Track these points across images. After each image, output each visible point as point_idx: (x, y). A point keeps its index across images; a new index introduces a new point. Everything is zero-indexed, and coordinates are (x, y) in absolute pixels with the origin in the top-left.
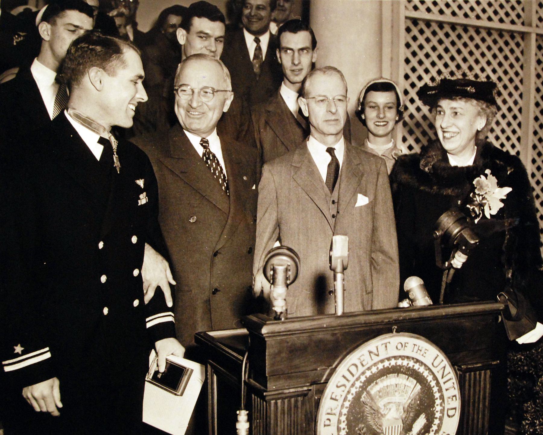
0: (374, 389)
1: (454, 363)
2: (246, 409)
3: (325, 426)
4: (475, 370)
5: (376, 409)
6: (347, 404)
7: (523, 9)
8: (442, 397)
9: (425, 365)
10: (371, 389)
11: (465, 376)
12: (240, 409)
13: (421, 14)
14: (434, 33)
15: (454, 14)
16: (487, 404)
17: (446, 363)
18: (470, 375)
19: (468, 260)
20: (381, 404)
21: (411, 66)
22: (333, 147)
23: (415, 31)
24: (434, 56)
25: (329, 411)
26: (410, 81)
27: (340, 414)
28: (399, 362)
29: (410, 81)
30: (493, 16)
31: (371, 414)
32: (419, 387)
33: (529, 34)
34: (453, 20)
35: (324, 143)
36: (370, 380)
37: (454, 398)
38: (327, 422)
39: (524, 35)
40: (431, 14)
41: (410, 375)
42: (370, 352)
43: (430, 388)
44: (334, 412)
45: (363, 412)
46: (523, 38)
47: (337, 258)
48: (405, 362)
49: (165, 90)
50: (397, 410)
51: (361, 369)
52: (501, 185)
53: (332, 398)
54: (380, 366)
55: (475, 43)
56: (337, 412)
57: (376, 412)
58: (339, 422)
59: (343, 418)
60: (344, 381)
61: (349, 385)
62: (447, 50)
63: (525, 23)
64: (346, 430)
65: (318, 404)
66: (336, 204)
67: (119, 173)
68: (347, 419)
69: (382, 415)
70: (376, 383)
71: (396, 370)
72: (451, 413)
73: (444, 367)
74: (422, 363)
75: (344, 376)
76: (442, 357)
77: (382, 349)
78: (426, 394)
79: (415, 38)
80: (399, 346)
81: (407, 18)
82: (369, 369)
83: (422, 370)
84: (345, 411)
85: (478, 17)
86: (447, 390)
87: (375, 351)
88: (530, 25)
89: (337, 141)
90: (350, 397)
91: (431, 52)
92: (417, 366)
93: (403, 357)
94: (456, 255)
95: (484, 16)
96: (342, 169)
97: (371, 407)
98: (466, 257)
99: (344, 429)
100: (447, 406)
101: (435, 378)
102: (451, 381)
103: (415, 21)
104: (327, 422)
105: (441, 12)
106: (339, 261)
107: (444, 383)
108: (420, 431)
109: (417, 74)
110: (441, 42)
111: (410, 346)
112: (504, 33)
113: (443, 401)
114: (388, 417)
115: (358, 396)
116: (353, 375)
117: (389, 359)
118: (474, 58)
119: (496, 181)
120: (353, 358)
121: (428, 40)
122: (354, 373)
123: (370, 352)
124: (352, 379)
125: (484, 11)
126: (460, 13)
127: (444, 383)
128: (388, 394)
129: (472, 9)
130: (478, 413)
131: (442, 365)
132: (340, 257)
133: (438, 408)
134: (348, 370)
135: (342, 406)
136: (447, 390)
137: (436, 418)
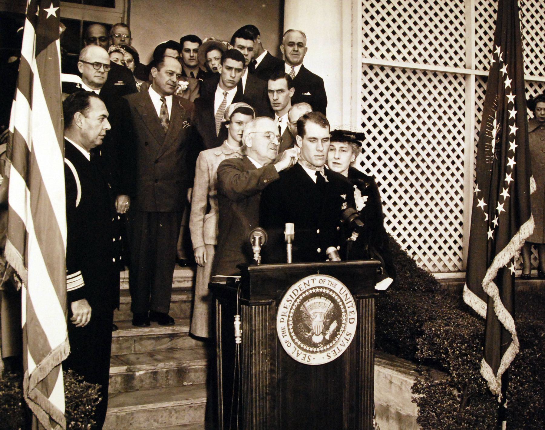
0: (307, 304)
1: (353, 293)
2: (239, 314)
3: (283, 336)
4: (366, 298)
5: (308, 315)
6: (293, 311)
8: (346, 312)
9: (336, 293)
10: (306, 304)
11: (360, 302)
12: (236, 314)
13: (377, 60)
14: (388, 76)
16: (373, 318)
17: (348, 292)
18: (363, 301)
19: (359, 236)
20: (311, 312)
23: (371, 74)
25: (283, 314)
26: (367, 116)
27: (289, 316)
28: (321, 290)
29: (367, 116)
31: (306, 318)
32: (332, 305)
36: (305, 299)
37: (353, 313)
38: (282, 320)
39: (465, 77)
41: (327, 298)
42: (305, 284)
43: (339, 306)
44: (285, 314)
45: (301, 316)
46: (464, 78)
47: (288, 235)
48: (324, 291)
50: (321, 317)
51: (300, 293)
52: (363, 195)
53: (284, 307)
54: (311, 292)
56: (287, 314)
57: (308, 317)
58: (288, 321)
59: (291, 319)
60: (290, 298)
61: (293, 300)
63: (466, 66)
64: (292, 325)
65: (277, 310)
67: (327, 181)
68: (293, 319)
69: (312, 319)
70: (309, 301)
71: (319, 294)
72: (352, 321)
73: (347, 295)
74: (334, 292)
75: (290, 296)
76: (345, 288)
77: (311, 282)
78: (337, 309)
79: (371, 80)
80: (321, 281)
82: (304, 292)
83: (334, 295)
84: (291, 315)
86: (348, 307)
87: (307, 283)
88: (470, 68)
90: (294, 307)
92: (331, 293)
93: (323, 288)
94: (353, 234)
97: (306, 314)
98: (358, 234)
99: (291, 325)
100: (349, 317)
101: (342, 300)
102: (351, 303)
103: (371, 67)
104: (282, 320)
106: (289, 237)
107: (347, 303)
108: (334, 330)
111: (327, 282)
113: (347, 314)
114: (315, 320)
115: (298, 307)
116: (296, 296)
117: (315, 288)
119: (360, 192)
120: (295, 286)
122: (296, 294)
123: (305, 284)
124: (295, 298)
127: (347, 303)
128: (315, 308)
130: (368, 324)
131: (345, 293)
132: (289, 235)
133: (344, 318)
134: (293, 292)
135: (290, 312)
136: (348, 307)
137: (343, 323)
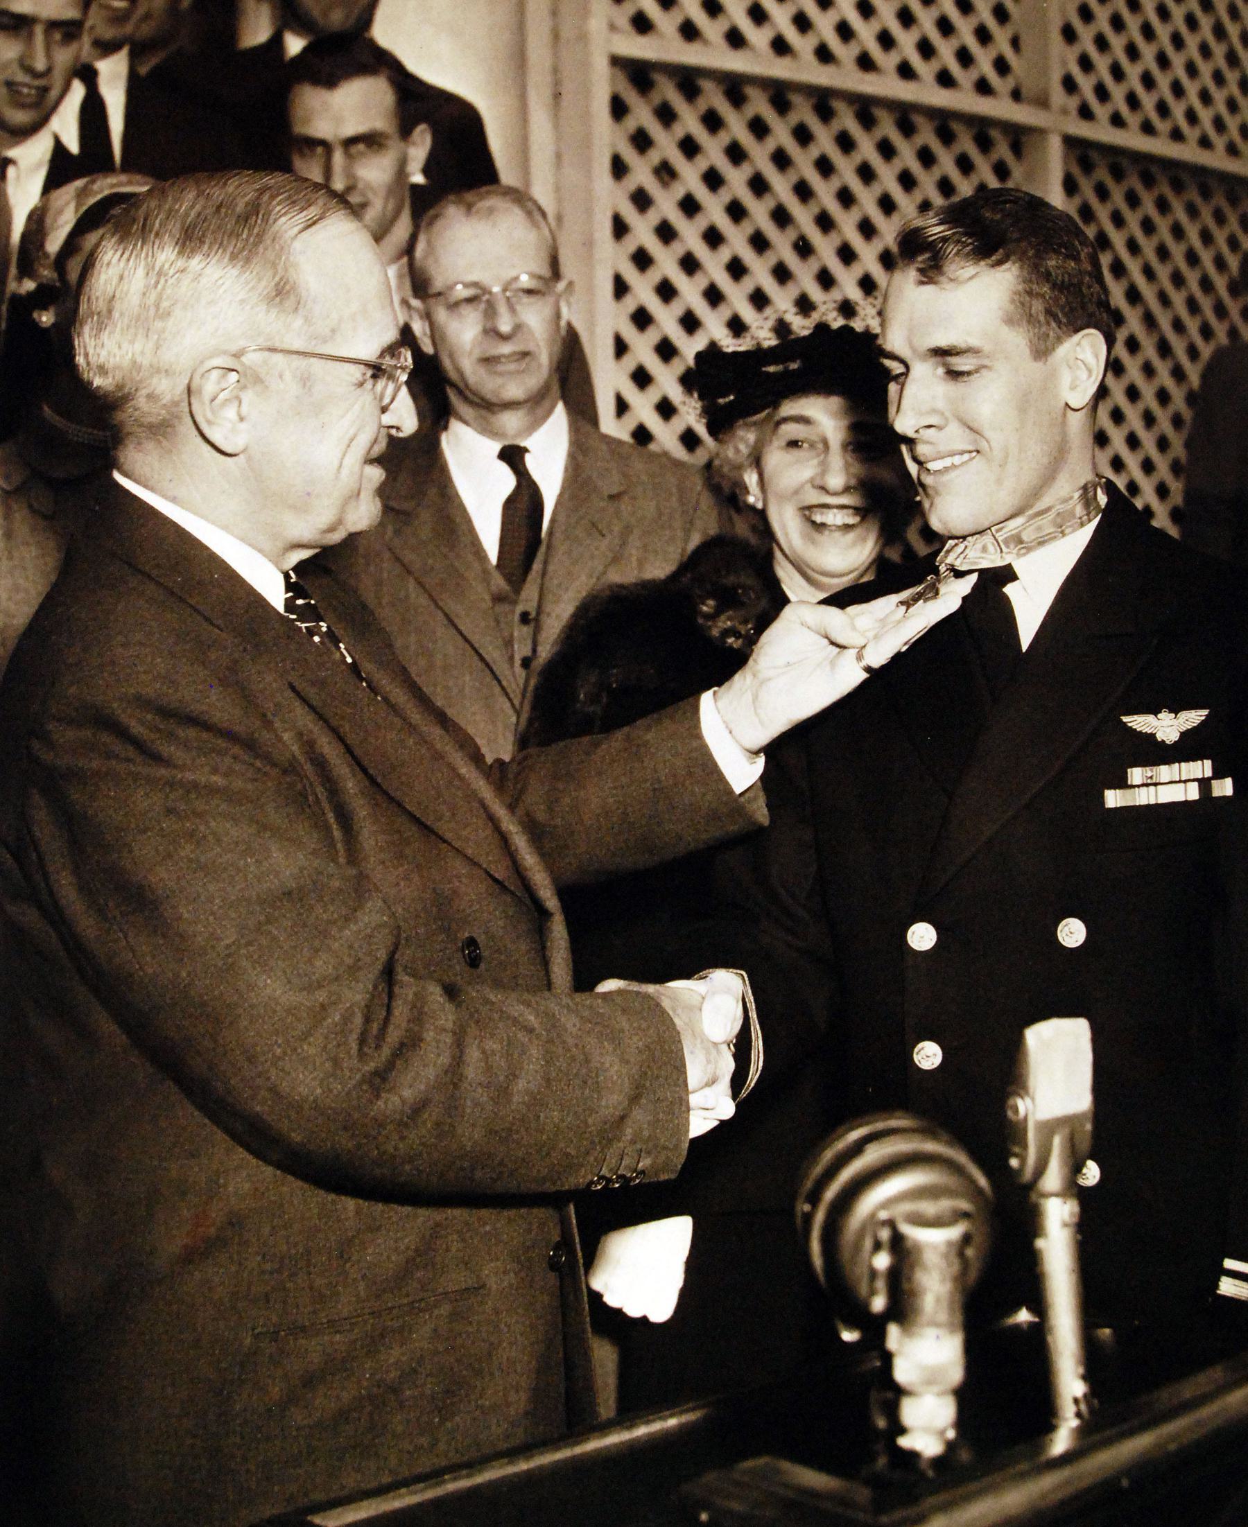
7: (1015, 43)
15: (780, 46)
21: (630, 245)
22: (522, 444)
24: (714, 210)
26: (630, 304)
30: (916, 60)
33: (1040, 132)
34: (780, 69)
35: (488, 431)
40: (696, 47)
46: (1017, 149)
49: (520, 1035)
55: (857, 158)
62: (759, 185)
63: (1024, 91)
66: (532, 625)
81: (617, 61)
85: (866, 63)
89: (536, 423)
91: (701, 193)
95: (887, 61)
96: (553, 521)
105: (735, 39)
109: (654, 276)
110: (736, 154)
112: (956, 127)
118: (677, 309)
121: (689, 147)
125: (886, 40)
126: (803, 45)
129: (845, 31)
